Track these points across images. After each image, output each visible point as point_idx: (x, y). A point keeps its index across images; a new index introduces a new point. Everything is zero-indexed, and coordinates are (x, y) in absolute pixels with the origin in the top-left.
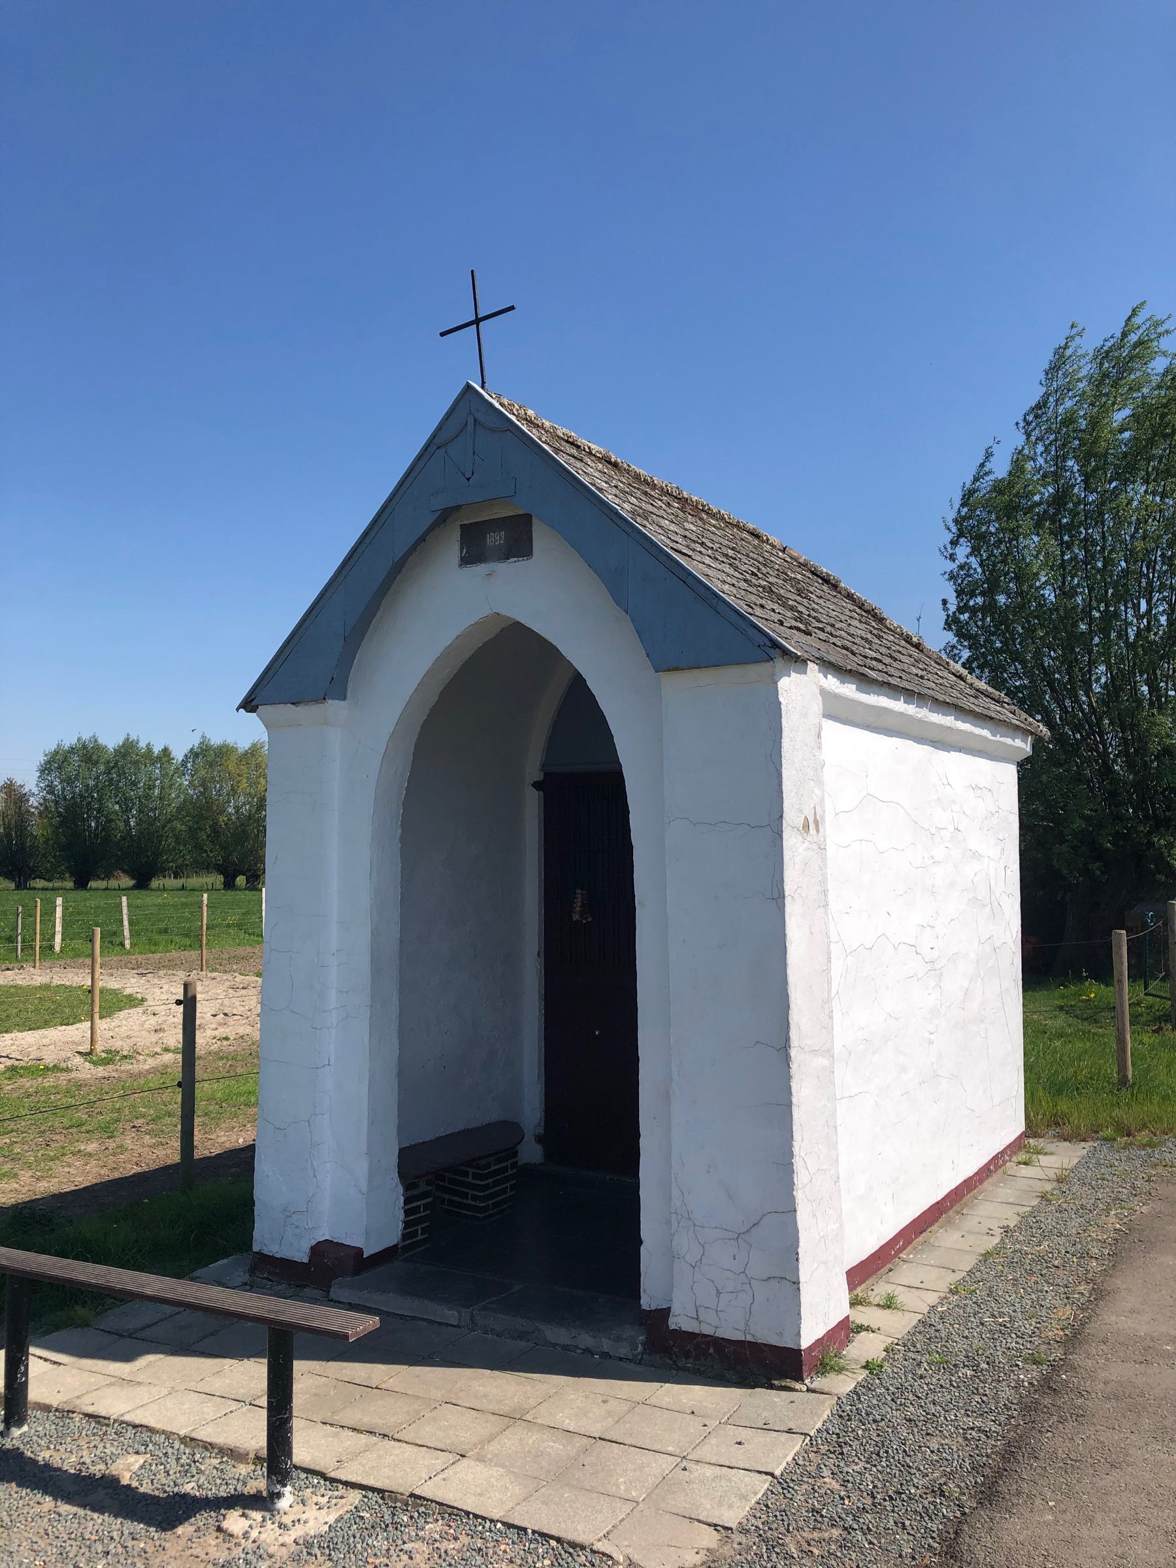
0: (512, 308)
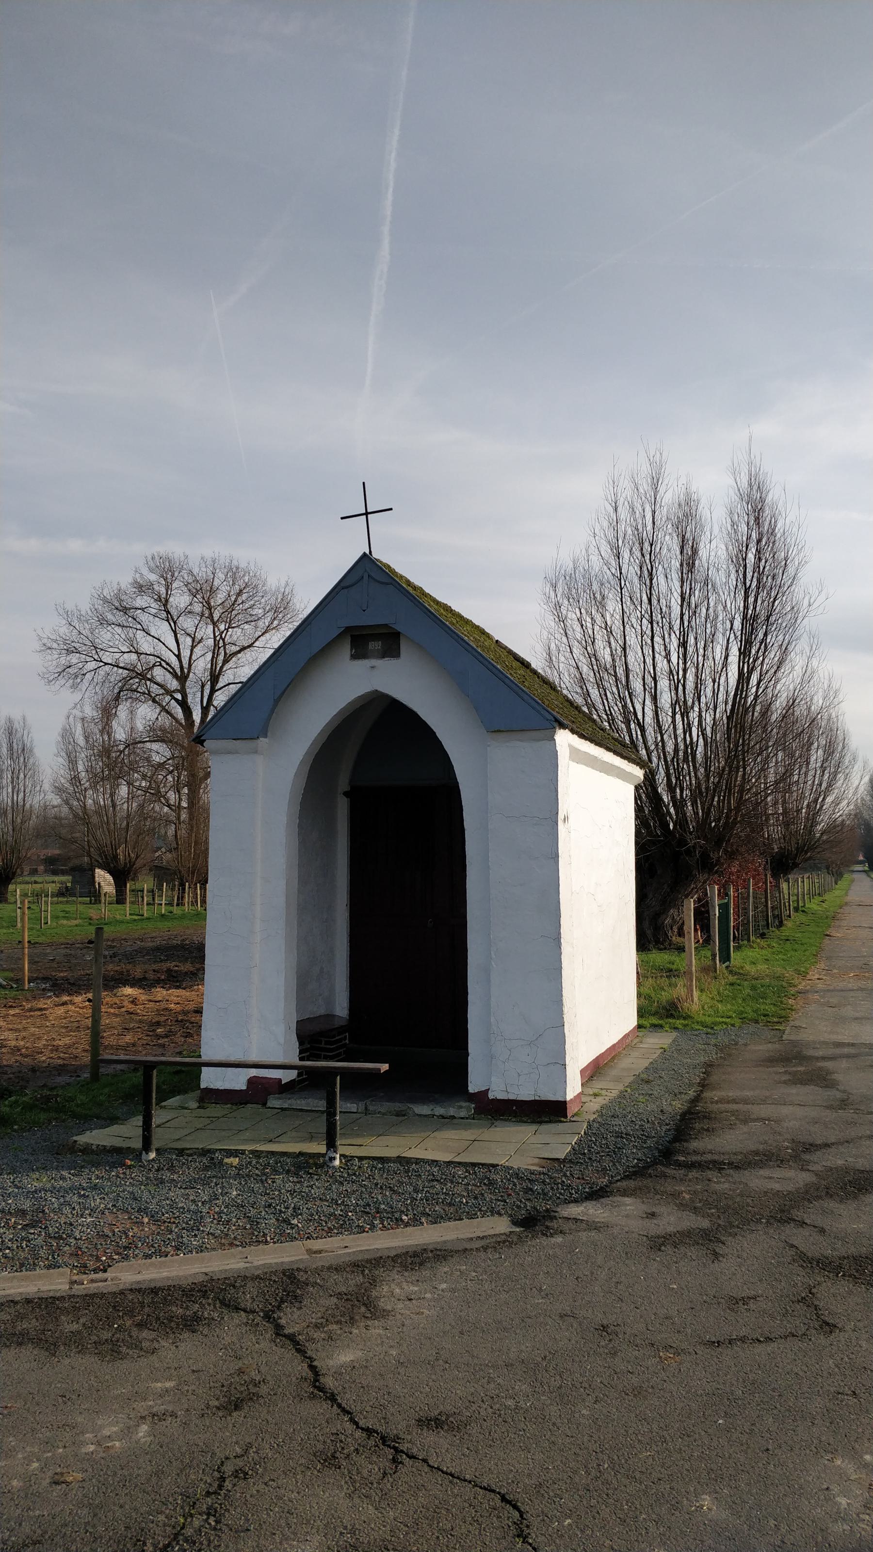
0: (391, 509)
